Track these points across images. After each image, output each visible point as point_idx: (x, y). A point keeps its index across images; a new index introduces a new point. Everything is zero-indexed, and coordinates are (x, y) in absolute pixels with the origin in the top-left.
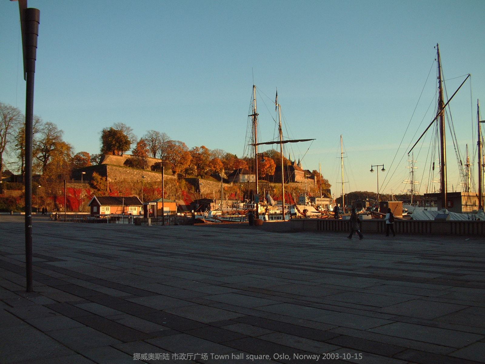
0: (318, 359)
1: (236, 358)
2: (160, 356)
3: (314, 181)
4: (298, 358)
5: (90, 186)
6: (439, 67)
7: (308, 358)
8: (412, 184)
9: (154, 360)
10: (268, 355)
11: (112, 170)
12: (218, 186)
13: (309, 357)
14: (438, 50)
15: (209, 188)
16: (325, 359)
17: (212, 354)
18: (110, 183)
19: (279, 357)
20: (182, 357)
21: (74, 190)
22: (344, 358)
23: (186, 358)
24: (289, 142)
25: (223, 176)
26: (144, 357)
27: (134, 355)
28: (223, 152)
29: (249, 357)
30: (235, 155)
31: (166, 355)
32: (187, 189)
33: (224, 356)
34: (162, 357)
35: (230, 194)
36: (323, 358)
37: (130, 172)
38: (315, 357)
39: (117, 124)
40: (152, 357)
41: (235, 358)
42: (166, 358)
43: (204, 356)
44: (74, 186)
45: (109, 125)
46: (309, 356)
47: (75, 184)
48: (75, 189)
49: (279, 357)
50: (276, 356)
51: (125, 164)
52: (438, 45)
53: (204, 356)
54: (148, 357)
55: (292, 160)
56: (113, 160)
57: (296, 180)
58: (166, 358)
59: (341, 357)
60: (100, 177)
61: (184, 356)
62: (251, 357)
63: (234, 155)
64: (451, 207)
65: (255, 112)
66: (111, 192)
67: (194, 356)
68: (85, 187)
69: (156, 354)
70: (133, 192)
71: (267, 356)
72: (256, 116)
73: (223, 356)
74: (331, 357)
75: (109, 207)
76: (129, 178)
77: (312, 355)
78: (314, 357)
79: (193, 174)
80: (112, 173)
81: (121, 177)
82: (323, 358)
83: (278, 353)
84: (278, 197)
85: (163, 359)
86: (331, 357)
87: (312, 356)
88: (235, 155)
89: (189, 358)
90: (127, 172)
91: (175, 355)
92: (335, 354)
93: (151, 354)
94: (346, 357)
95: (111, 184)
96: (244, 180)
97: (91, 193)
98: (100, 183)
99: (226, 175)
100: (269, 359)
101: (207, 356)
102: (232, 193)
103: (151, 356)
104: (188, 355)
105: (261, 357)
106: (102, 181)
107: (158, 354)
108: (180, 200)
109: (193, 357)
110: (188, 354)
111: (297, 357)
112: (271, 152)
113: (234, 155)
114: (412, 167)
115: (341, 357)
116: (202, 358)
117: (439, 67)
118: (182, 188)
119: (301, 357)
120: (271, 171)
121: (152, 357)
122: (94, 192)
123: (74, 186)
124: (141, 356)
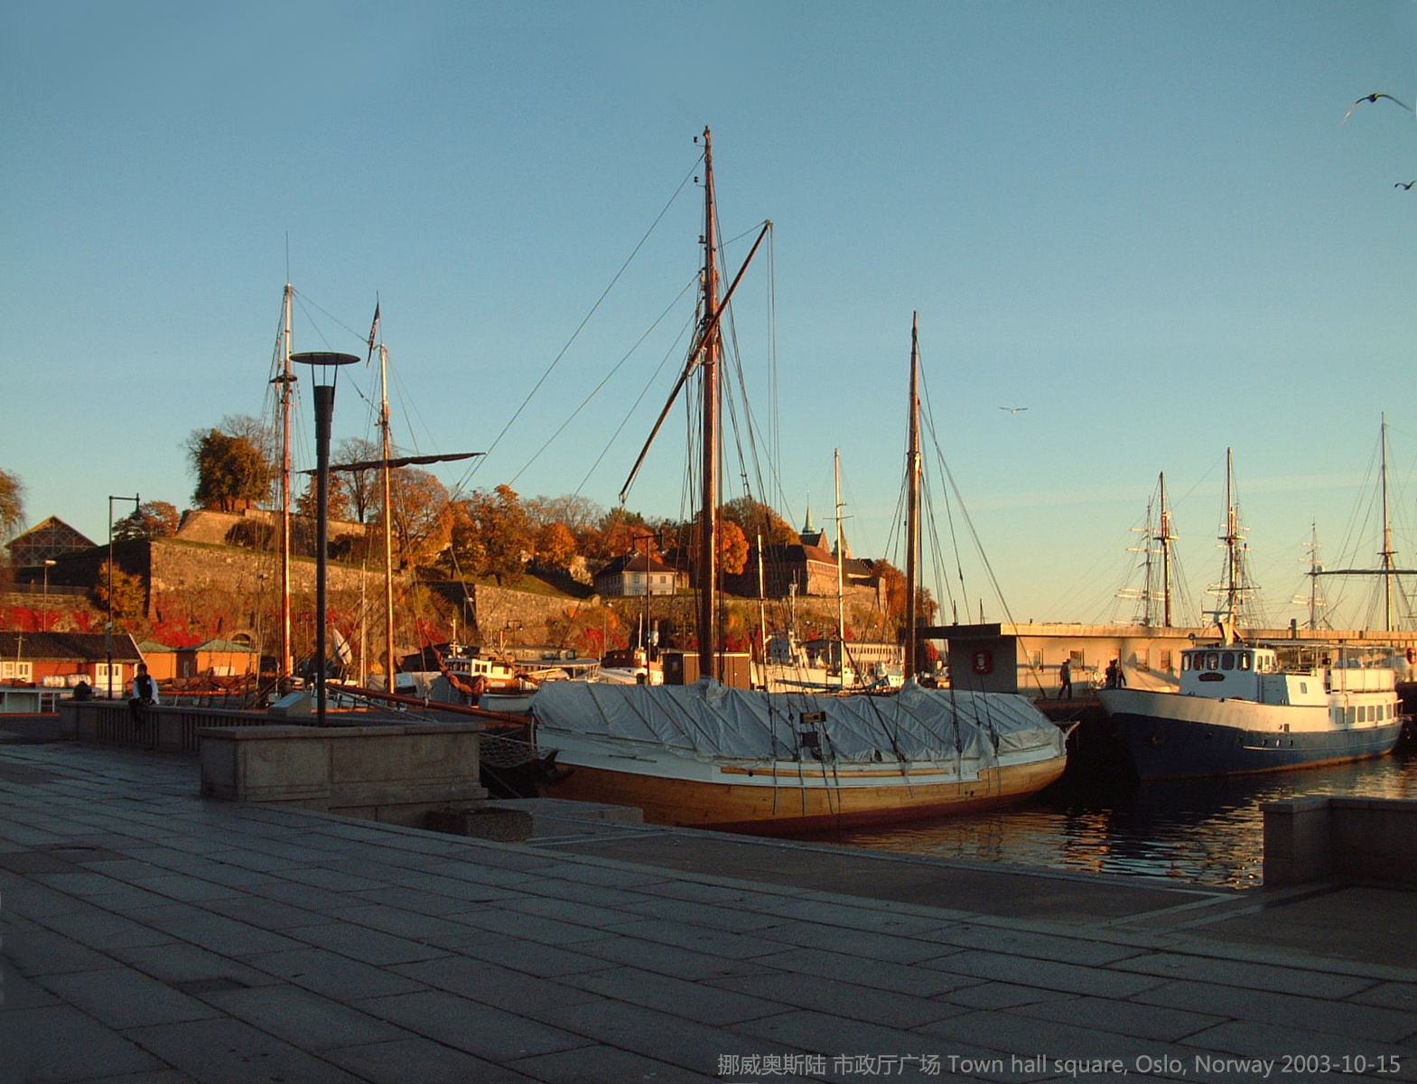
0: (1269, 1071)
1: (1023, 1070)
2: (796, 1062)
3: (878, 593)
4: (1208, 1070)
5: (91, 604)
6: (709, 203)
7: (1239, 1070)
8: (1148, 600)
9: (781, 1074)
10: (1120, 1062)
11: (170, 554)
12: (544, 605)
13: (1242, 1066)
14: (707, 147)
15: (511, 611)
16: (1290, 1071)
17: (954, 1057)
18: (158, 594)
19: (1154, 1068)
20: (864, 1067)
21: (33, 614)
22: (1380, 1069)
23: (875, 1069)
24: (439, 462)
25: (581, 575)
26: (750, 1065)
27: (721, 1059)
28: (589, 505)
29: (1064, 1067)
30: (639, 514)
31: (817, 1061)
32: (435, 616)
33: (989, 1061)
34: (804, 1065)
35: (582, 630)
36: (1284, 1070)
37: (234, 562)
38: (1260, 1065)
39: (233, 418)
40: (774, 1067)
41: (1021, 1071)
42: (817, 1071)
43: (930, 1062)
44: (35, 601)
45: (213, 419)
46: (1242, 1062)
47: (38, 595)
48: (36, 610)
49: (1154, 1068)
50: (1144, 1064)
51: (228, 536)
52: (707, 132)
53: (930, 1062)
54: (761, 1066)
55: (813, 529)
56: (214, 525)
57: (808, 592)
58: (817, 1071)
59: (1338, 1065)
60: (122, 575)
61: (869, 1062)
62: (1068, 1067)
63: (636, 514)
64: (986, 673)
65: (285, 371)
66: (160, 621)
67: (899, 1062)
68: (74, 605)
69: (786, 1057)
70: (240, 622)
71: (1117, 1064)
72: (291, 384)
73: (986, 1063)
74: (1308, 1066)
75: (30, 665)
76: (229, 581)
77: (1249, 1062)
78: (1258, 1066)
79: (474, 568)
80: (169, 564)
81: (201, 577)
82: (1284, 1070)
83: (1135, 1060)
84: (740, 641)
85: (807, 1071)
86: (1308, 1066)
87: (1252, 1065)
88: (639, 514)
89: (884, 1067)
90: (225, 560)
91: (841, 1060)
92: (1319, 1057)
93: (771, 1056)
94: (1352, 1066)
95: (162, 596)
96: (636, 590)
97: (93, 623)
98: (123, 594)
99: (589, 575)
100: (1123, 1071)
101: (939, 1063)
102: (592, 626)
103: (772, 1063)
104: (882, 1059)
105: (1099, 1065)
106: (127, 589)
107: (792, 1057)
108: (408, 648)
109: (895, 1067)
110: (880, 1057)
111: (1200, 1063)
112: (742, 505)
113: (636, 514)
114: (1146, 551)
115: (1338, 1065)
116: (924, 1068)
117: (709, 203)
118: (416, 612)
119: (1219, 1066)
120: (736, 561)
121: (774, 1067)
122: (101, 622)
123: (35, 601)
124: (740, 1063)
